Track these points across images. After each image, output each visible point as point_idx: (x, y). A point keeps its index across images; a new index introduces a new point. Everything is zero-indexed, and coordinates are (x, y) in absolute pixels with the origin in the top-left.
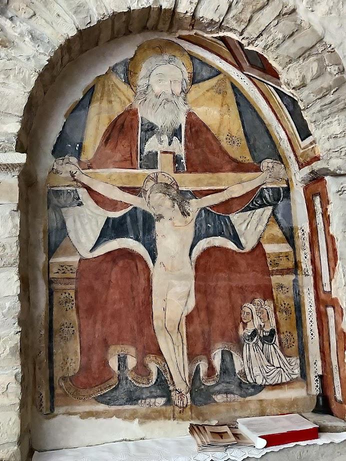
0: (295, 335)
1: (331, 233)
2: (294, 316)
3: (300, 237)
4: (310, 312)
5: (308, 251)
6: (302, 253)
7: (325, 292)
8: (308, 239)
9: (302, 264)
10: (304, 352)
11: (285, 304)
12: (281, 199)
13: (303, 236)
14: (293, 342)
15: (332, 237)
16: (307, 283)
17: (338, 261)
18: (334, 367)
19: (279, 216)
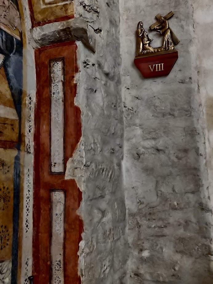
0: (11, 230)
1: (76, 104)
2: (11, 203)
3: (27, 106)
4: (28, 198)
5: (32, 123)
6: (27, 125)
7: (51, 174)
8: (34, 110)
9: (26, 138)
10: (17, 251)
11: (4, 188)
12: (14, 51)
13: (30, 105)
14: (8, 240)
15: (77, 111)
16: (29, 160)
17: (82, 137)
18: (55, 263)
19: (10, 70)
